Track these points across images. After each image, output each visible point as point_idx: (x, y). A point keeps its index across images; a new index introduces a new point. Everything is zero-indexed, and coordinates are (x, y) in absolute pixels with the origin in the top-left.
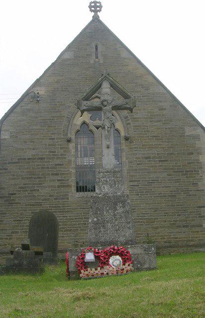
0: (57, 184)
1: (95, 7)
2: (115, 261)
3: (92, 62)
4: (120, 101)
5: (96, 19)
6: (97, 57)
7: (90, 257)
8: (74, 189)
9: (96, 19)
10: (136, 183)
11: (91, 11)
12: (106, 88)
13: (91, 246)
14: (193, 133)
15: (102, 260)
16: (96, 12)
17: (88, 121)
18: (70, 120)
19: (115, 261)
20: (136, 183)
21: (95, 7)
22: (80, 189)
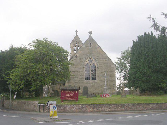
0: (81, 78)
1: (90, 33)
2: (107, 96)
3: (89, 48)
4: (107, 76)
5: (90, 36)
6: (90, 46)
7: (104, 95)
8: (85, 79)
9: (90, 36)
10: (99, 78)
11: (89, 34)
12: (105, 74)
13: (104, 94)
14: (113, 67)
15: (106, 96)
16: (90, 34)
17: (88, 63)
18: (84, 62)
19: (107, 96)
20: (99, 78)
21: (90, 33)
22: (86, 79)
